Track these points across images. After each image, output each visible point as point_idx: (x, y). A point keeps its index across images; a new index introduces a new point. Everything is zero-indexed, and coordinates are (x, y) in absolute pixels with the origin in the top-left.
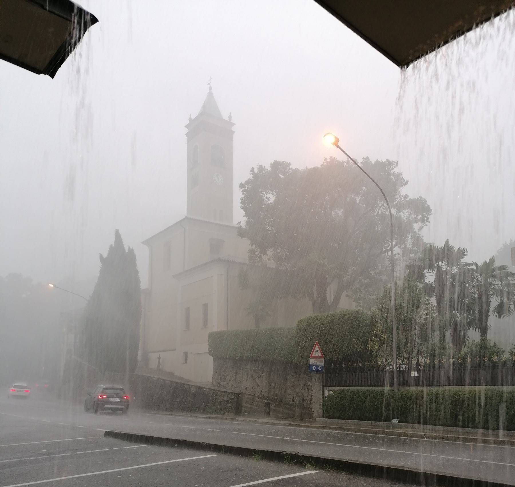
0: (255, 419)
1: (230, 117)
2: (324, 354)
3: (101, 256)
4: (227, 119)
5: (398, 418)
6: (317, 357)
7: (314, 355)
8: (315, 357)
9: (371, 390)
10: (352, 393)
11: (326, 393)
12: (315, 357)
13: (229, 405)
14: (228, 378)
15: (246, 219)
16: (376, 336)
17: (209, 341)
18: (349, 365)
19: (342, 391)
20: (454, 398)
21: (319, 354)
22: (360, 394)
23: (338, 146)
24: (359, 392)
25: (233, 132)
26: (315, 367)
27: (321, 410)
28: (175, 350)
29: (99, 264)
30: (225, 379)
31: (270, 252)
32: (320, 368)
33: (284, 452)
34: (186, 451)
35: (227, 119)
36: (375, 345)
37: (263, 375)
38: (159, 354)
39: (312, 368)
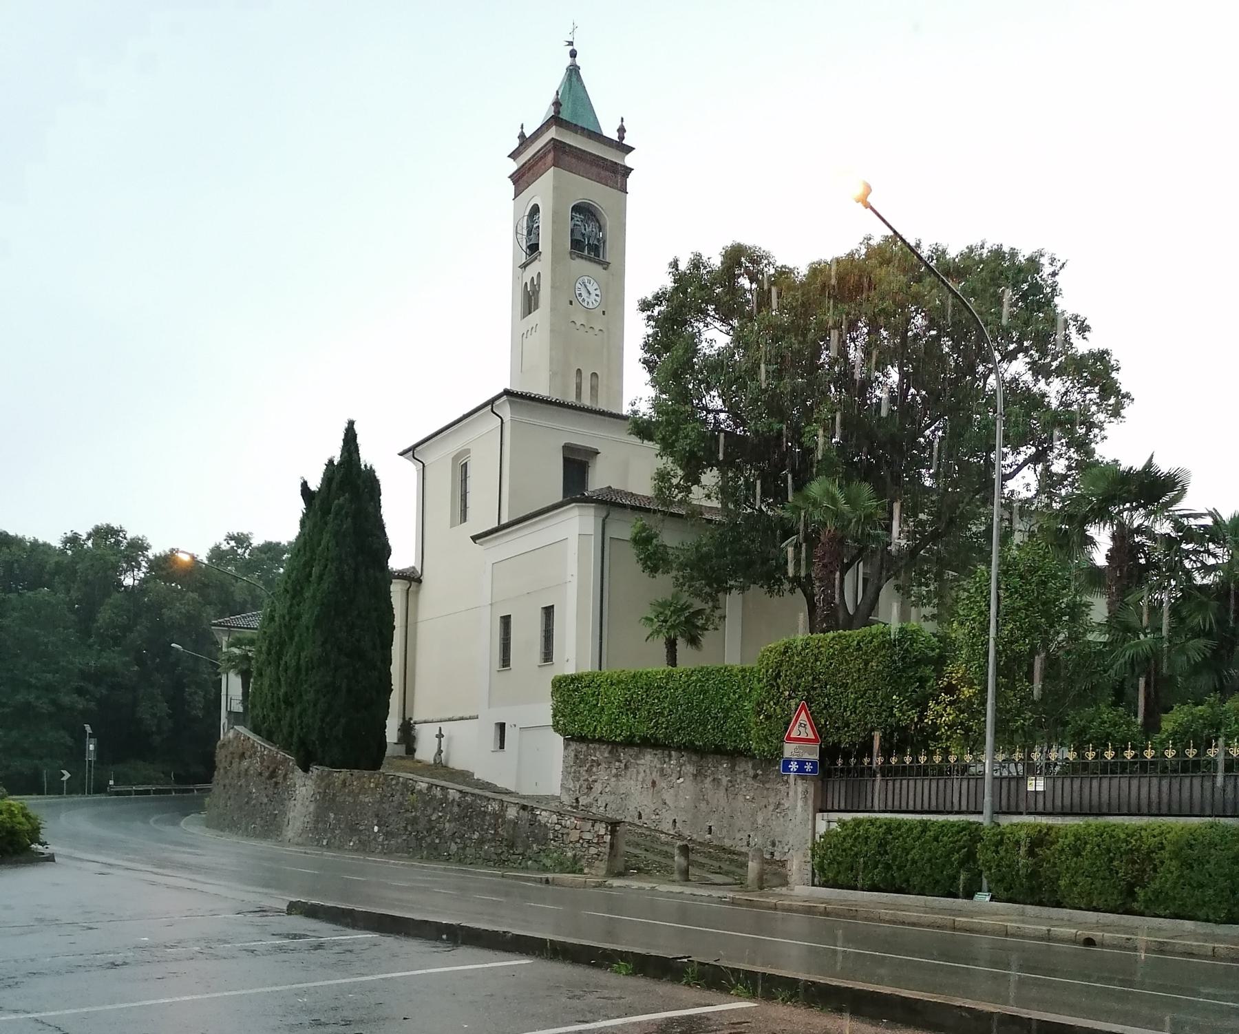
0: (651, 885)
2: (820, 731)
5: (989, 891)
9: (929, 823)
10: (884, 827)
19: (858, 823)
20: (1127, 845)
22: (903, 830)
23: (868, 206)
24: (900, 824)
25: (627, 171)
31: (710, 477)
33: (685, 957)
34: (464, 951)
36: (946, 711)
37: (679, 781)
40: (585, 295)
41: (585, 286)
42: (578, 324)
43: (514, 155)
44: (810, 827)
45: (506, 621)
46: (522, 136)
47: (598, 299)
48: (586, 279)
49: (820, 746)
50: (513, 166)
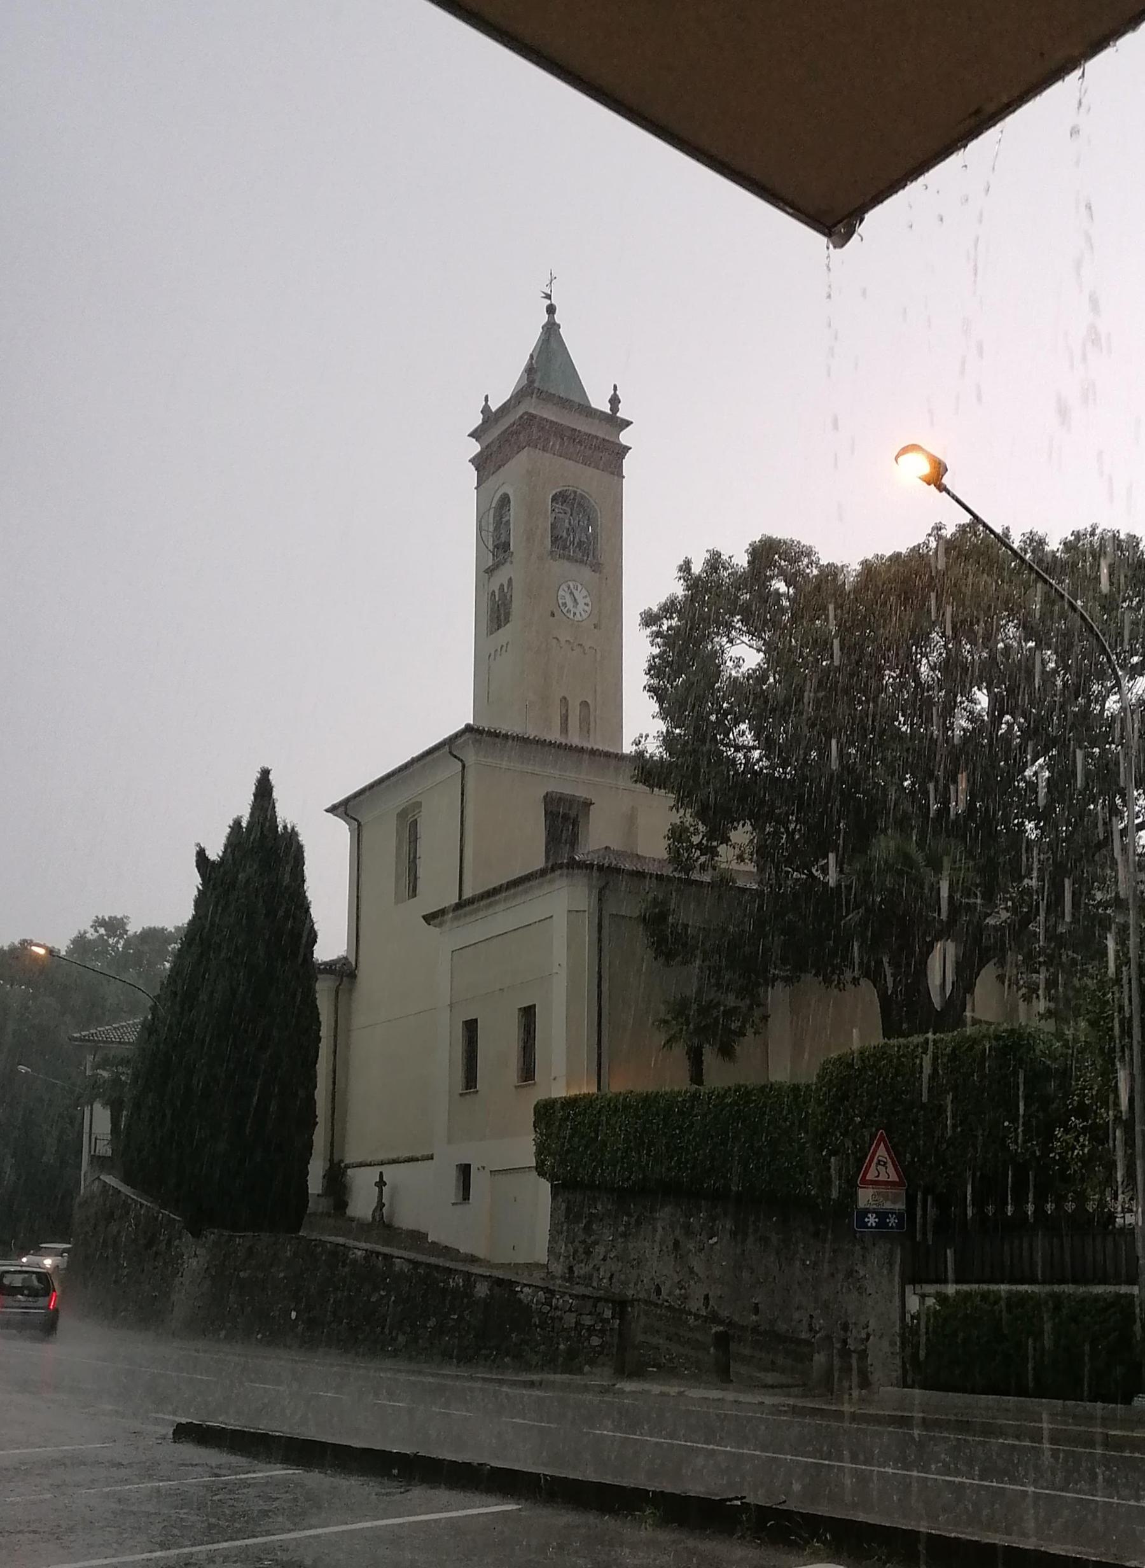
1: (615, 401)
3: (201, 854)
4: (607, 408)
6: (886, 1183)
8: (875, 1183)
11: (913, 1304)
12: (875, 1183)
13: (595, 1341)
15: (661, 726)
16: (1082, 1112)
17: (537, 1130)
21: (890, 1174)
23: (942, 488)
27: (898, 1361)
28: (432, 1159)
29: (194, 881)
30: (588, 1253)
31: (742, 834)
32: (892, 1221)
33: (737, 1498)
35: (607, 408)
36: (1078, 1141)
39: (867, 1220)
40: (570, 604)
41: (571, 593)
43: (475, 435)
45: (471, 1027)
46: (486, 410)
47: (588, 609)
49: (907, 1190)
50: (475, 448)
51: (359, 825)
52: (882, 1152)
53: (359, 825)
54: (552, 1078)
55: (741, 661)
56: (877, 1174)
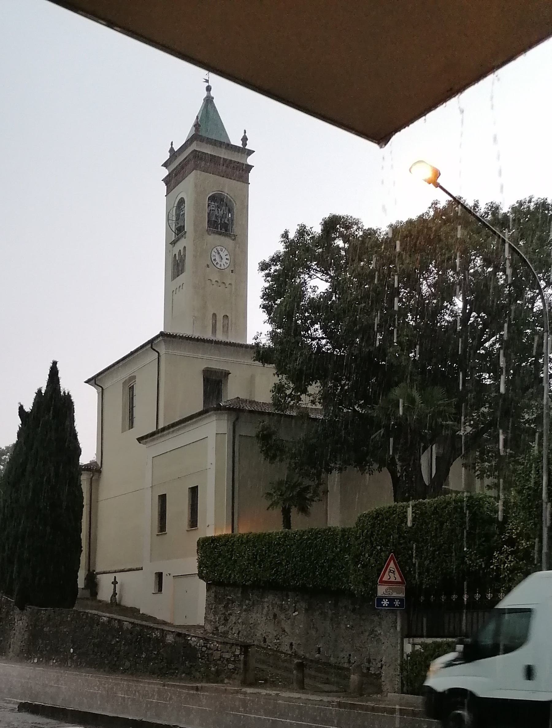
0: (275, 692)
1: (245, 139)
3: (21, 408)
4: (239, 144)
7: (385, 578)
11: (408, 649)
14: (232, 620)
15: (269, 328)
18: (454, 597)
23: (437, 185)
25: (250, 167)
26: (398, 601)
29: (18, 422)
37: (294, 614)
38: (115, 577)
40: (218, 260)
41: (219, 253)
42: (214, 281)
43: (166, 165)
44: (399, 648)
45: (163, 498)
46: (172, 150)
47: (228, 262)
48: (219, 248)
50: (165, 172)
51: (102, 389)
52: (392, 565)
53: (102, 389)
54: (207, 525)
55: (316, 288)
56: (389, 577)
